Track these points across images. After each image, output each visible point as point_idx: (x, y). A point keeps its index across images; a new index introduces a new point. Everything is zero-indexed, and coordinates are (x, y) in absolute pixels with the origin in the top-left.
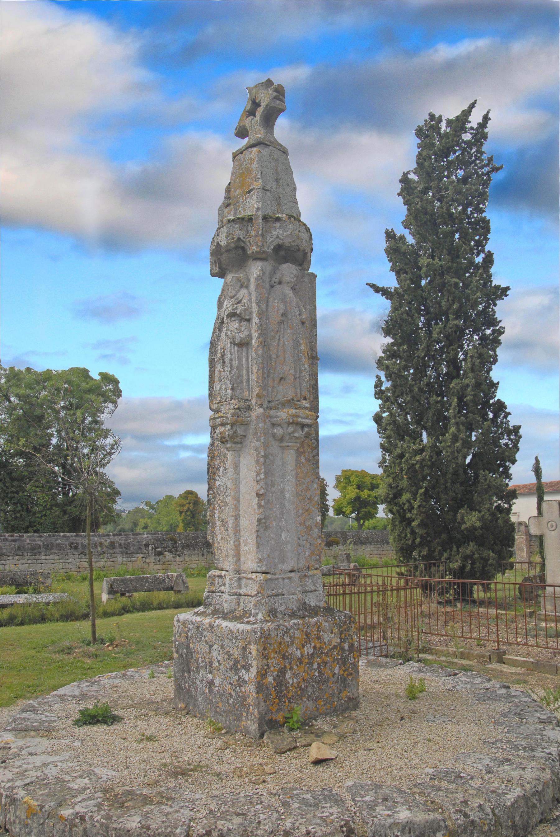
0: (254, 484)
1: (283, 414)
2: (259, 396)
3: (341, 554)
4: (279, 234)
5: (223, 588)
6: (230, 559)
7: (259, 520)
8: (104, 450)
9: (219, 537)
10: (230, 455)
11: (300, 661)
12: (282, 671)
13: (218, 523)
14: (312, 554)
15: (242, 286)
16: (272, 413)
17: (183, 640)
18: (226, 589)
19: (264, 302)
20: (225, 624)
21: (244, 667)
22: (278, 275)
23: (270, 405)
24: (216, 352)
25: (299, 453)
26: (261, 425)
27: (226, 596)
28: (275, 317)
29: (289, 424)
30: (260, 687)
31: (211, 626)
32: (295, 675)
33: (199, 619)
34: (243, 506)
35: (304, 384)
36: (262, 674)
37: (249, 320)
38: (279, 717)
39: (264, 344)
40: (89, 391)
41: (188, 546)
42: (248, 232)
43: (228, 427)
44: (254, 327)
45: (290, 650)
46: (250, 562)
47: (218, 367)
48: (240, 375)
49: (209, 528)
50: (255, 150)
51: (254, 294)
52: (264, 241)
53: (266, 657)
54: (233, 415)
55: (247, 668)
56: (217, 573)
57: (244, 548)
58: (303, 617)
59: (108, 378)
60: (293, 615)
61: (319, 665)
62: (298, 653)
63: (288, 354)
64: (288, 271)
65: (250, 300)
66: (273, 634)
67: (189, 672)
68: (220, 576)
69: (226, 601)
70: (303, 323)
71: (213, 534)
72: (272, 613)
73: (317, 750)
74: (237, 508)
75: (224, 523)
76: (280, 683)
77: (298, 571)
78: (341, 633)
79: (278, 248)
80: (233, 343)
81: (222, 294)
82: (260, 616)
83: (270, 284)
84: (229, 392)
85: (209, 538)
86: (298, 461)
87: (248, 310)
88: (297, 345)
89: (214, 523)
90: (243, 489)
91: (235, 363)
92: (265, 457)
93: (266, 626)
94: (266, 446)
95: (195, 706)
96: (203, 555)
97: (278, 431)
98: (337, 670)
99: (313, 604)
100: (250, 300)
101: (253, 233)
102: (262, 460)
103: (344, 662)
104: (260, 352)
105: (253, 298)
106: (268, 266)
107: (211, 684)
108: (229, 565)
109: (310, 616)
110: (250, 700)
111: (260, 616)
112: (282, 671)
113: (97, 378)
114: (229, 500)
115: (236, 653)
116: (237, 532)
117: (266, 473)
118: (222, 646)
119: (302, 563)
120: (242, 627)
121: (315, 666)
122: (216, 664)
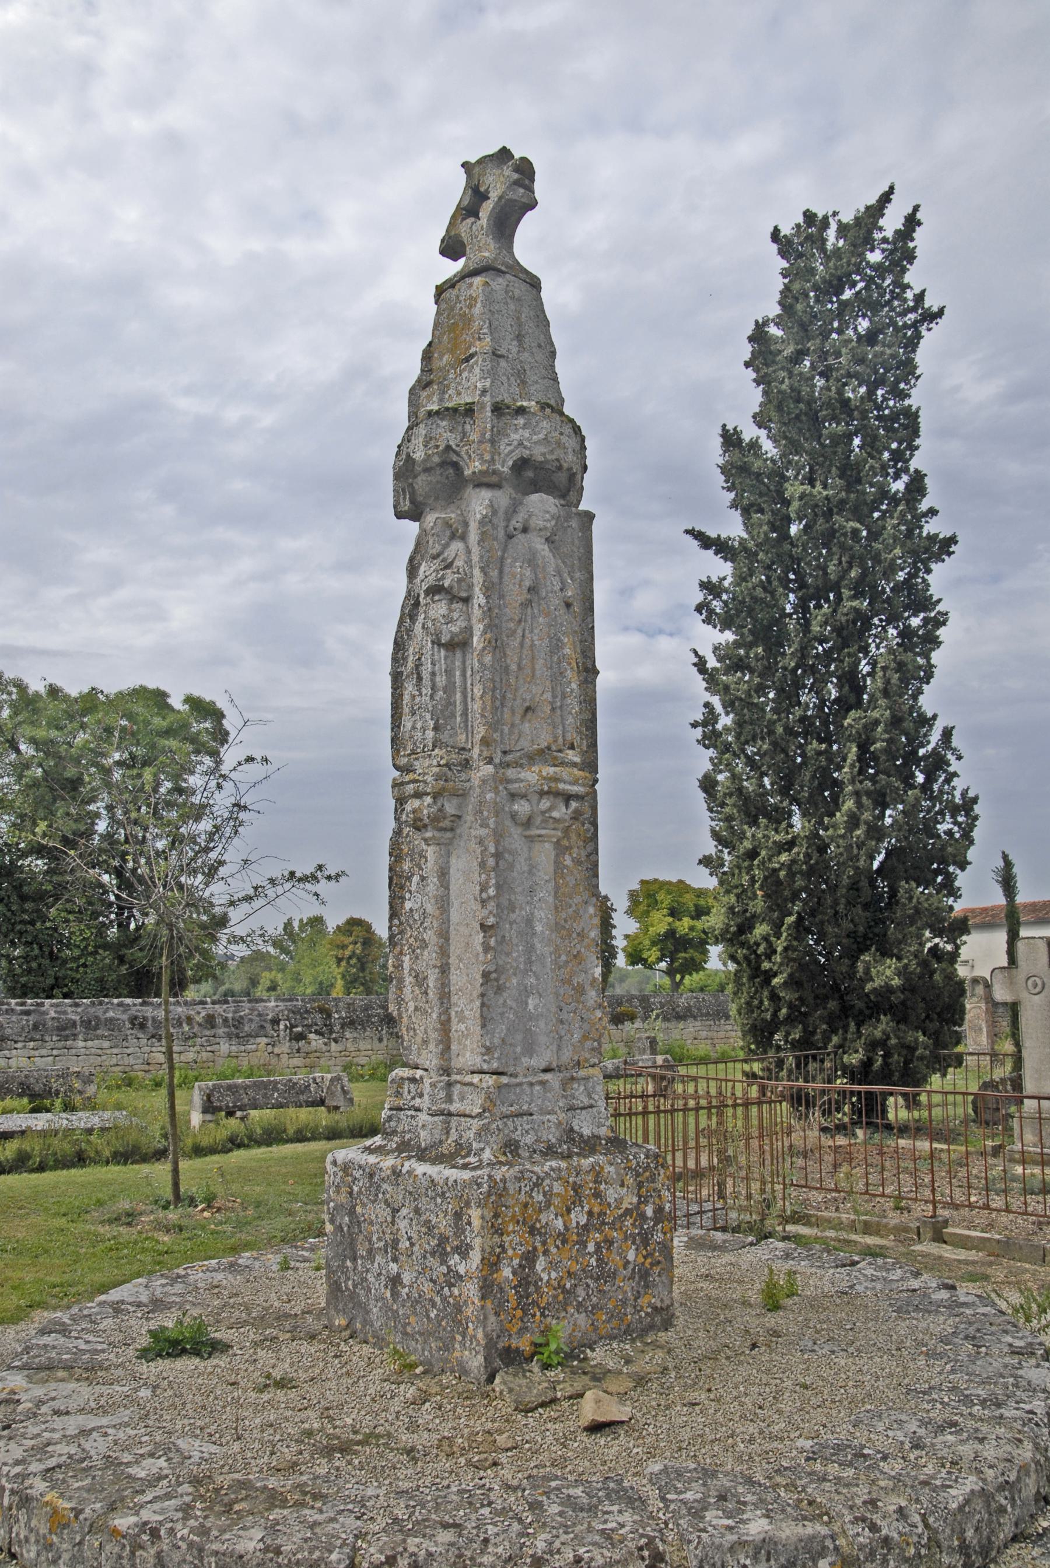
1: (531, 776)
2: (485, 742)
3: (640, 1039)
4: (525, 438)
5: (417, 1102)
6: (432, 1046)
8: (195, 843)
9: (411, 1006)
11: (563, 1237)
12: (530, 1258)
13: (409, 980)
14: (585, 1037)
15: (453, 537)
16: (511, 773)
18: (424, 1103)
19: (495, 565)
21: (457, 1250)
26: (489, 796)
27: (423, 1117)
28: (515, 594)
29: (542, 794)
30: (487, 1289)
31: (396, 1173)
32: (552, 1265)
33: (372, 1159)
34: (455, 948)
35: (570, 720)
36: (491, 1263)
37: (466, 600)
38: (523, 1344)
39: (496, 645)
41: (352, 1023)
42: (464, 434)
43: (428, 800)
44: (477, 613)
45: (544, 1218)
47: (409, 688)
48: (450, 703)
50: (478, 280)
54: (438, 777)
56: (406, 1073)
57: (457, 1027)
59: (200, 707)
60: (550, 1151)
61: (598, 1246)
62: (559, 1224)
63: (540, 664)
64: (541, 506)
65: (469, 562)
67: (354, 1259)
68: (413, 1080)
69: (425, 1128)
70: (568, 605)
74: (444, 952)
75: (420, 980)
76: (525, 1280)
78: (640, 1185)
80: (437, 643)
82: (487, 1155)
84: (430, 734)
87: (465, 580)
88: (556, 646)
89: (401, 980)
91: (441, 680)
93: (499, 1174)
94: (498, 836)
95: (365, 1322)
96: (380, 1040)
97: (522, 808)
98: (631, 1256)
99: (586, 1132)
100: (469, 562)
102: (491, 862)
104: (488, 659)
105: (475, 558)
106: (503, 498)
107: (395, 1281)
108: (429, 1058)
112: (530, 1258)
114: (430, 936)
115: (444, 1224)
116: (445, 996)
117: (498, 887)
118: (417, 1211)
119: (567, 1055)
120: (453, 1174)
121: (591, 1247)
122: (404, 1244)
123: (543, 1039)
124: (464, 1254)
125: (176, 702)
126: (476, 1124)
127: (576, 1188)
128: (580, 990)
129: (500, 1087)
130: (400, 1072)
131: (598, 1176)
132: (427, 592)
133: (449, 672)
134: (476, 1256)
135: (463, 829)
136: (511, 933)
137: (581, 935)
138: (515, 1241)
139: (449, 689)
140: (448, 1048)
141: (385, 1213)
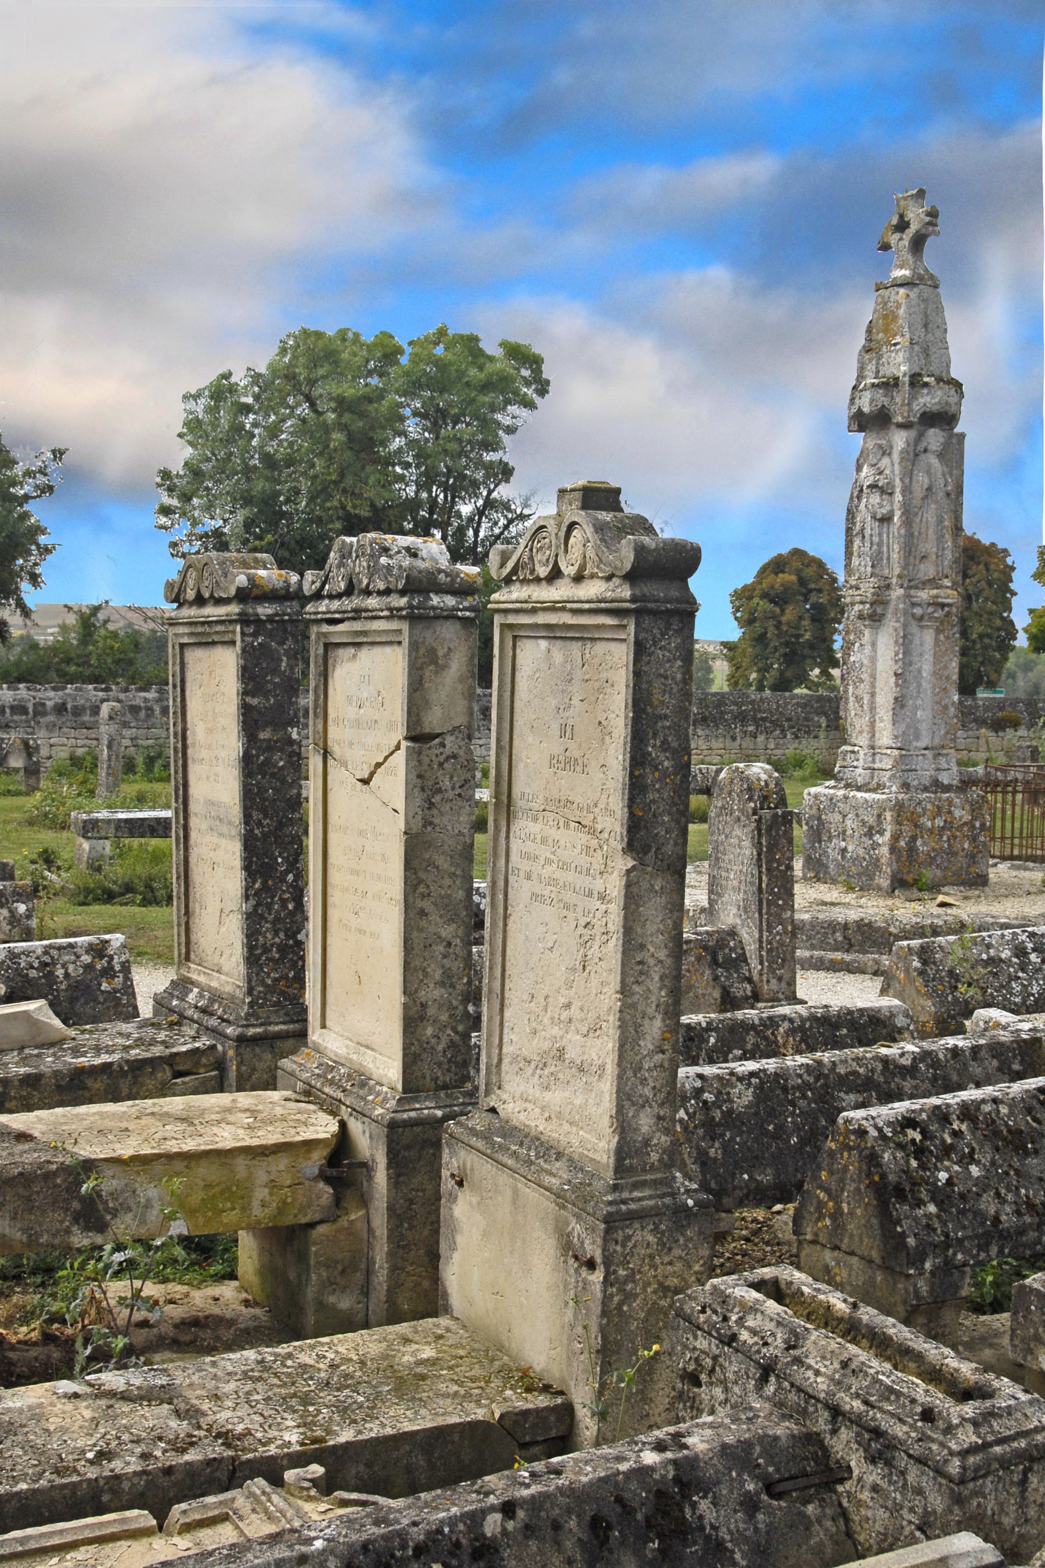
0: (892, 663)
1: (924, 595)
2: (900, 576)
3: (1020, 747)
4: (928, 400)
5: (855, 763)
6: (865, 734)
7: (896, 699)
8: (509, 510)
9: (853, 713)
10: (867, 632)
11: (931, 831)
12: (914, 838)
13: (851, 699)
14: (947, 733)
15: (884, 454)
16: (913, 592)
17: (814, 812)
18: (861, 763)
19: (908, 474)
20: (859, 795)
21: (878, 832)
22: (923, 445)
23: (911, 583)
24: (854, 524)
25: (938, 631)
26: (901, 606)
27: (860, 771)
28: (918, 492)
29: (929, 604)
30: (893, 849)
31: (846, 797)
32: (924, 844)
33: (832, 791)
34: (879, 684)
35: (946, 563)
36: (895, 838)
37: (891, 494)
38: (909, 878)
39: (908, 520)
40: (486, 387)
41: (704, 719)
42: (892, 398)
43: (868, 606)
44: (897, 506)
45: (922, 820)
46: (885, 737)
47: (857, 542)
48: (880, 552)
49: (842, 703)
50: (902, 291)
51: (897, 467)
52: (910, 410)
53: (900, 824)
54: (873, 594)
55: (881, 833)
56: (849, 748)
57: (879, 725)
58: (935, 792)
59: (519, 354)
60: (926, 789)
61: (949, 839)
62: (929, 824)
63: (931, 531)
64: (934, 437)
65: (893, 472)
66: (907, 804)
67: (820, 842)
68: (853, 752)
69: (860, 775)
70: (948, 495)
71: (846, 710)
72: (906, 786)
73: (941, 898)
74: (873, 685)
75: (858, 699)
76: (911, 849)
77: (933, 749)
78: (973, 810)
79: (924, 415)
80: (874, 517)
81: (861, 456)
82: (894, 789)
83: (914, 455)
84: (869, 569)
85: (842, 713)
86: (936, 639)
87: (891, 484)
88: (940, 521)
89: (847, 699)
90: (880, 667)
91: (876, 539)
92: (904, 637)
93: (900, 797)
94: (905, 626)
95: (825, 873)
96: (734, 739)
97: (918, 611)
98: (966, 845)
99: (946, 782)
100: (893, 472)
101: (898, 400)
102: (901, 641)
103: (974, 839)
104: (903, 531)
105: (897, 472)
106: (912, 434)
107: (844, 850)
108: (863, 740)
109: (943, 792)
110: (884, 860)
111: (894, 789)
112: (914, 838)
113: (497, 352)
114: (864, 676)
115: (871, 820)
116: (873, 708)
117: (904, 653)
118: (857, 815)
119: (937, 741)
120: (877, 796)
121: (945, 838)
122: (849, 832)
123: (924, 733)
124: (882, 834)
125: (491, 347)
126: (889, 773)
127: (939, 807)
128: (946, 707)
129: (901, 756)
130: (845, 748)
131: (950, 803)
132: (868, 487)
133: (880, 535)
134: (888, 835)
135: (886, 621)
136: (910, 677)
137: (948, 678)
138: (907, 830)
139: (880, 544)
140: (874, 736)
141: (840, 818)
